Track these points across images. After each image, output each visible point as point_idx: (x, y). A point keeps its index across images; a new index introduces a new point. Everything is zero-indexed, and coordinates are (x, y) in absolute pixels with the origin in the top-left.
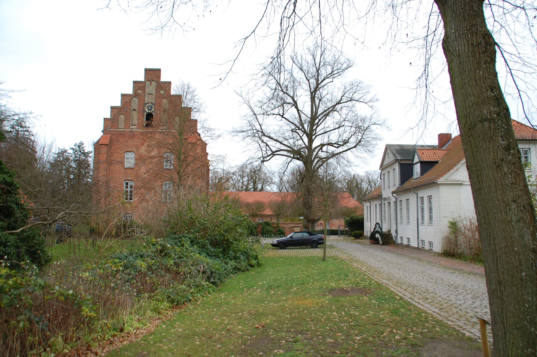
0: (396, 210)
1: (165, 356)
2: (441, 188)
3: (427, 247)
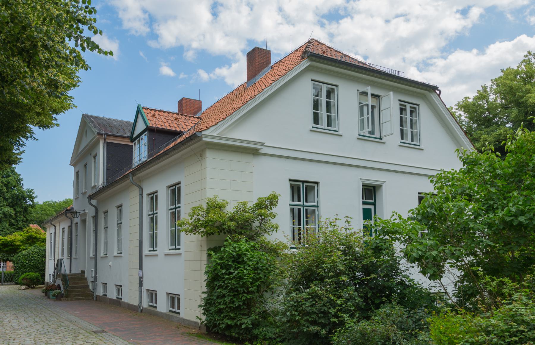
0: (96, 232)
1: (13, 344)
2: (211, 157)
3: (162, 306)
